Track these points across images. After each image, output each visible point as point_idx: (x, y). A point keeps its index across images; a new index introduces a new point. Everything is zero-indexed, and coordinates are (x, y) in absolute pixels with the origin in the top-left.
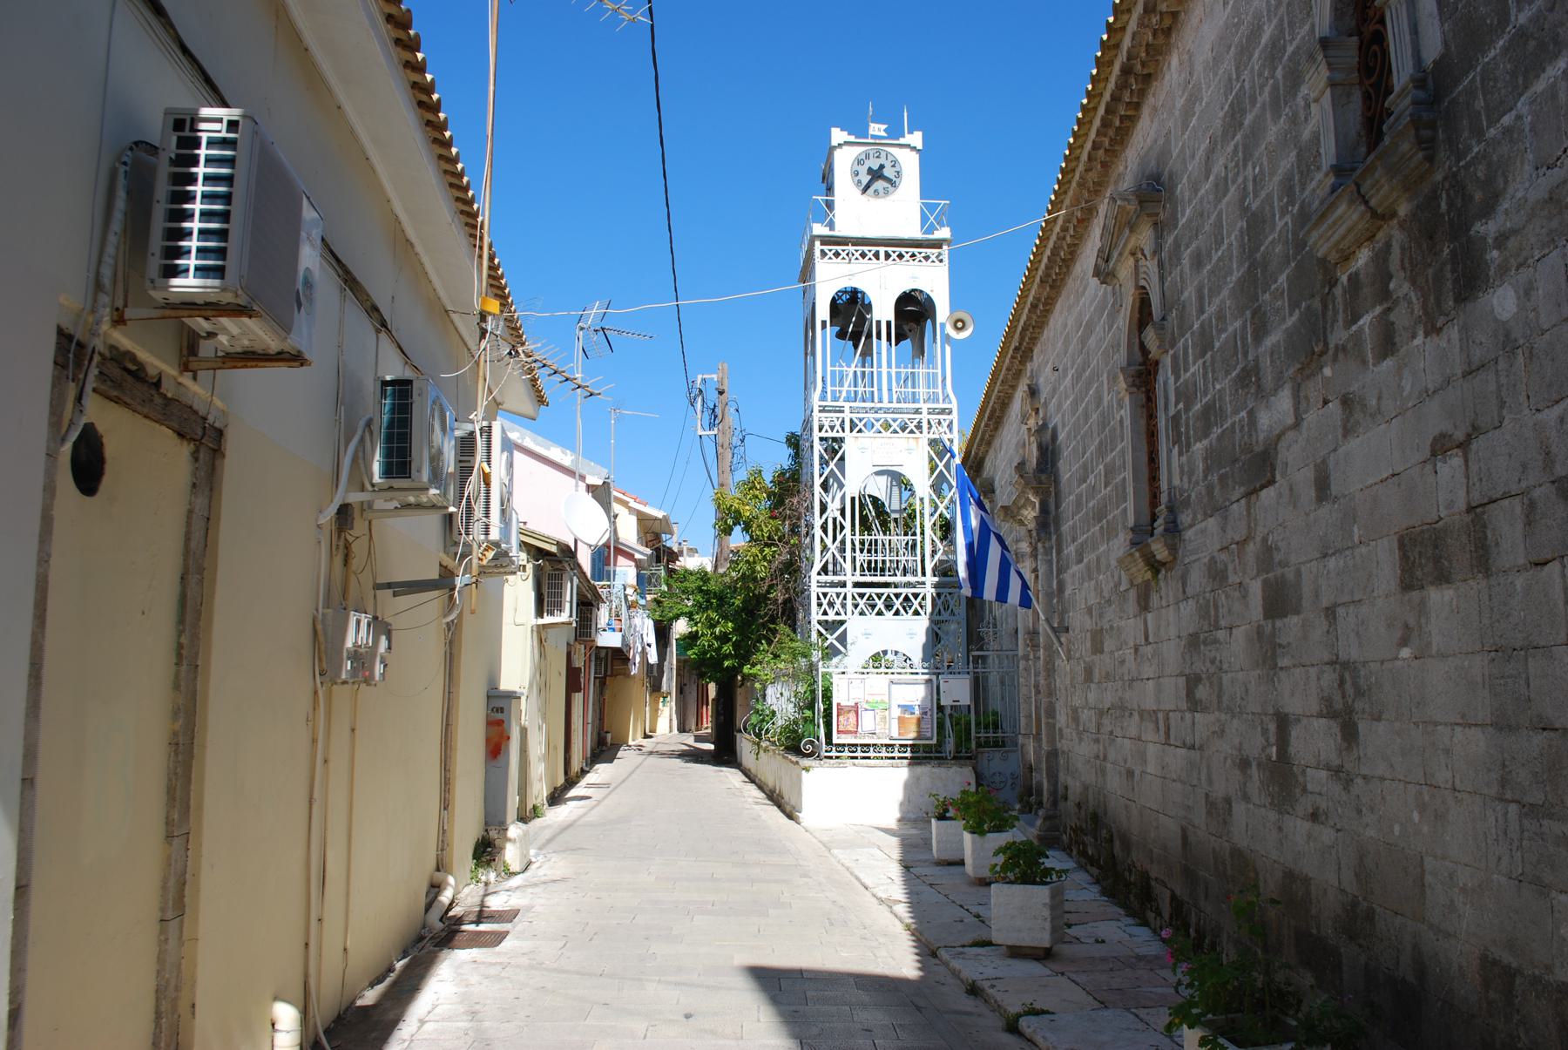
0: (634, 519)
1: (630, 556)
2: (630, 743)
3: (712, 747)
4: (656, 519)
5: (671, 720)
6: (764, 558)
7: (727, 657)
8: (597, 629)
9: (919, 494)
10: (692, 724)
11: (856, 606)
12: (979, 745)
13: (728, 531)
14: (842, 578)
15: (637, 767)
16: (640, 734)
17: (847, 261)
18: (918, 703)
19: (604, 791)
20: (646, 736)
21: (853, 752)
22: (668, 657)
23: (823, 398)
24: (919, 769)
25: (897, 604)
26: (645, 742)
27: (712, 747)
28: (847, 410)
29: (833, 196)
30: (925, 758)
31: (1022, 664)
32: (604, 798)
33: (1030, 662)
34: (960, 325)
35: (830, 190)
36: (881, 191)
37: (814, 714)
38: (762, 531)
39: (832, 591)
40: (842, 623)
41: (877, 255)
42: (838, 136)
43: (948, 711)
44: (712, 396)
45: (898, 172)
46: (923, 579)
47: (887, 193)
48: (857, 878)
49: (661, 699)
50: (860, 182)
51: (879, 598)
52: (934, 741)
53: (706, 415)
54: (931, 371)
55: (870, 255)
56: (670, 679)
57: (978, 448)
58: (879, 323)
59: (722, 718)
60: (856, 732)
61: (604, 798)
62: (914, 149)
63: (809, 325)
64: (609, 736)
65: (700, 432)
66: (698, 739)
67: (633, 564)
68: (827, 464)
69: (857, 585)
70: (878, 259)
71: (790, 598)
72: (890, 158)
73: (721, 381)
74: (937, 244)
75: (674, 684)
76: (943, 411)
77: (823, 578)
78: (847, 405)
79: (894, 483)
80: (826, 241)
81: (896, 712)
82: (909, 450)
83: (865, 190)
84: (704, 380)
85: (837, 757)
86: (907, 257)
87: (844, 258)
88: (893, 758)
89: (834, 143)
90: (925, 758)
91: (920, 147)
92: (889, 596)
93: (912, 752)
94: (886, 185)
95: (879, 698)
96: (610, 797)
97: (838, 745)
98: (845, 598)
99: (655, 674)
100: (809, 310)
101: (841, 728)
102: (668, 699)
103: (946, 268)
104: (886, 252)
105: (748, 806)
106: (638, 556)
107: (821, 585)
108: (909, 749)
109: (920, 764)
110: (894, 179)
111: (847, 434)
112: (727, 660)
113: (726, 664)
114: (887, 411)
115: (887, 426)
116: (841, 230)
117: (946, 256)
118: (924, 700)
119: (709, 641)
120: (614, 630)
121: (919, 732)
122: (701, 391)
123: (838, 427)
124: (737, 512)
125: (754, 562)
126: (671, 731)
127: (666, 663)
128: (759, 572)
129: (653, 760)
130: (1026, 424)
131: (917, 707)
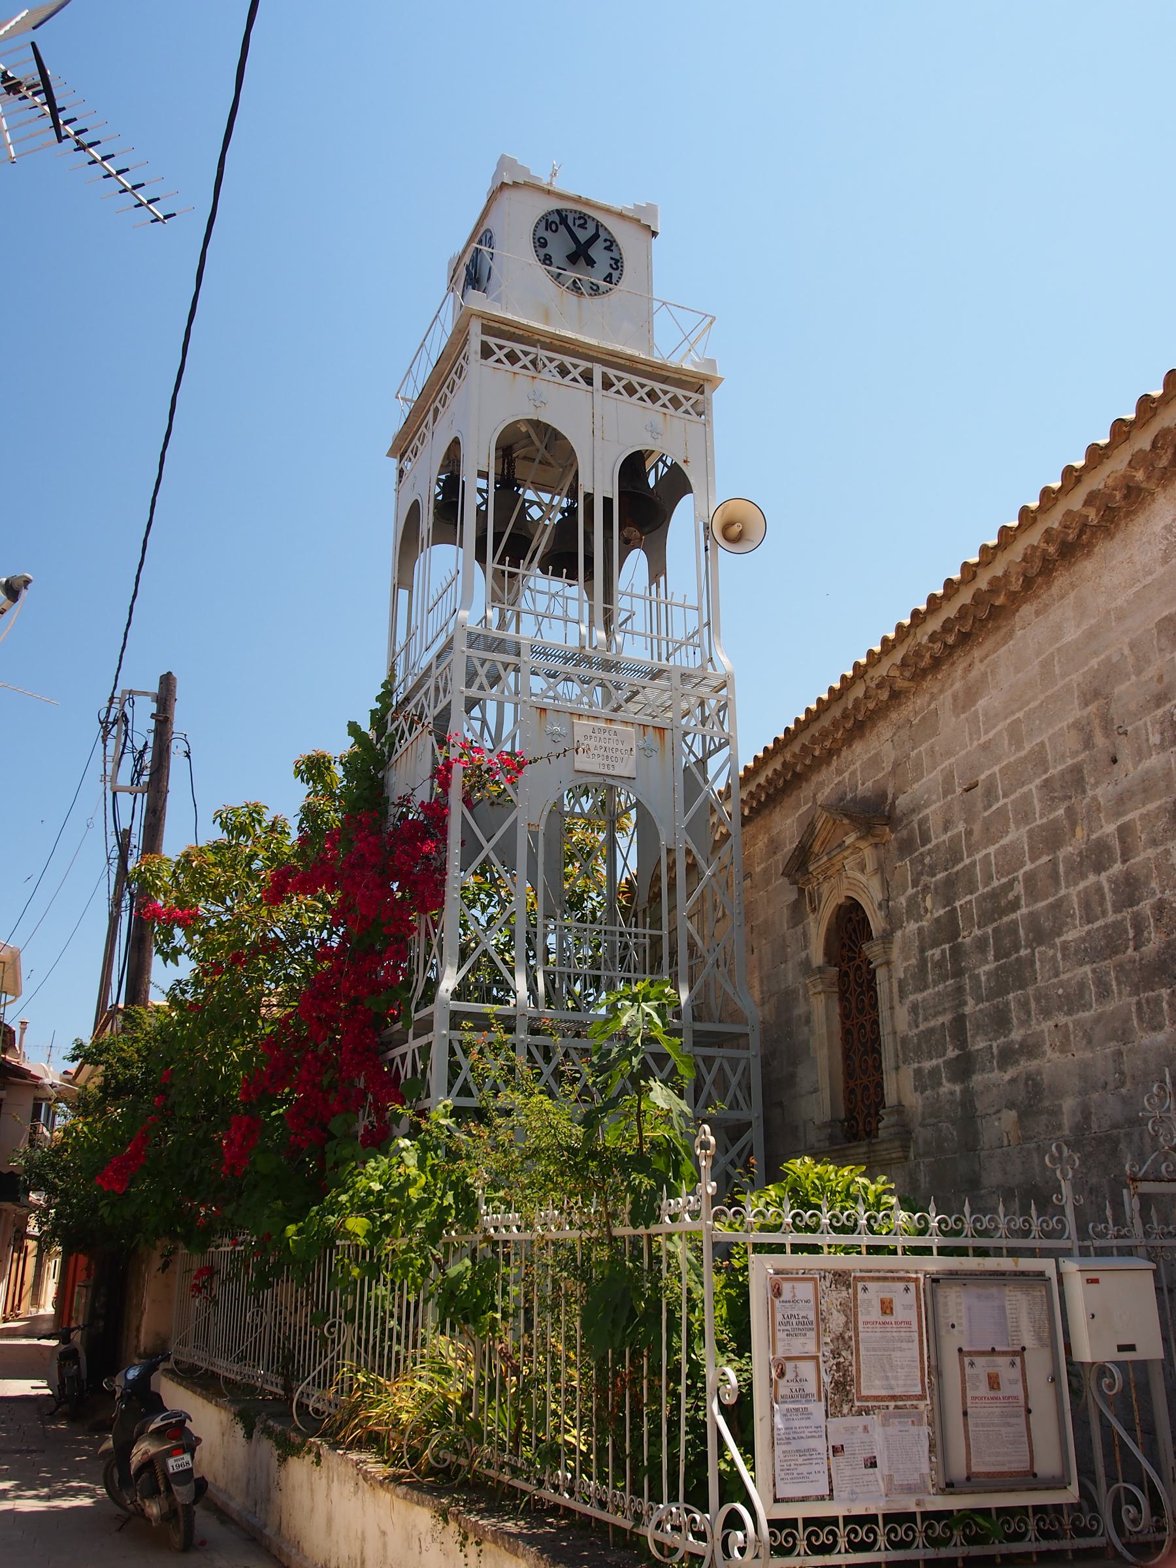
45: (617, 261)
52: (1071, 1494)
58: (589, 497)
59: (101, 1324)
92: (494, 666)
104: (604, 375)
126: (132, 784)
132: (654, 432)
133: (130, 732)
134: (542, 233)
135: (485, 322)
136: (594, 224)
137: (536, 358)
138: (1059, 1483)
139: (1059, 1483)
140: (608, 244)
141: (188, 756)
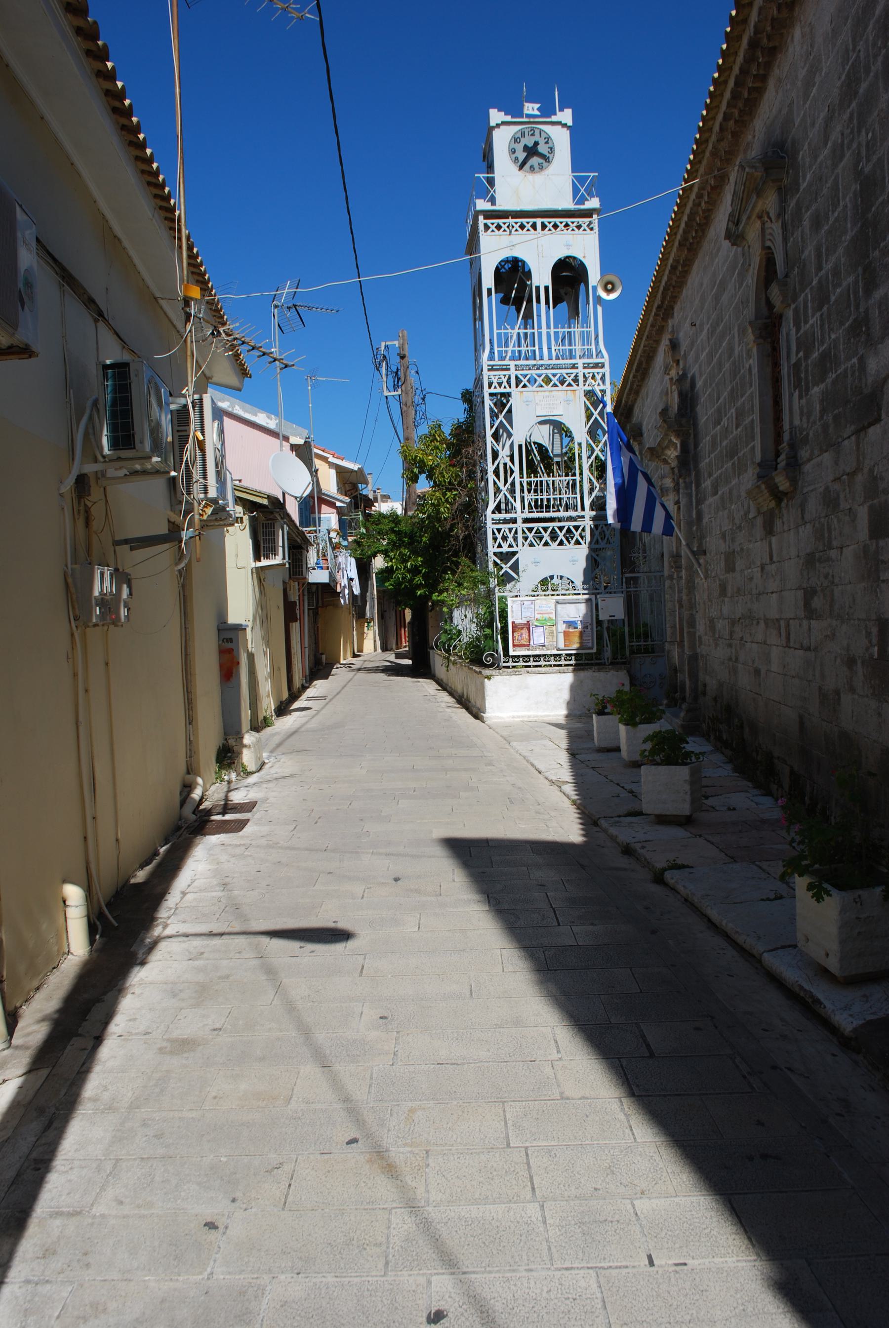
0: (333, 472)
1: (332, 505)
2: (342, 661)
3: (409, 662)
4: (352, 471)
5: (375, 641)
7: (419, 587)
8: (307, 568)
9: (577, 439)
11: (526, 539)
12: (632, 652)
13: (414, 479)
16: (349, 654)
17: (508, 233)
18: (580, 619)
21: (526, 662)
22: (369, 589)
23: (491, 358)
24: (582, 674)
26: (354, 660)
27: (409, 662)
28: (512, 368)
29: (494, 173)
30: (587, 664)
32: (322, 708)
33: (675, 581)
34: (609, 287)
35: (490, 168)
36: (536, 166)
37: (493, 631)
38: (444, 477)
40: (514, 554)
41: (534, 226)
43: (605, 625)
44: (395, 361)
45: (551, 148)
46: (583, 513)
47: (541, 168)
48: (532, 765)
49: (366, 625)
50: (517, 159)
52: (594, 650)
53: (390, 377)
55: (528, 226)
56: (372, 608)
57: (628, 398)
58: (538, 288)
60: (528, 645)
61: (322, 708)
62: (564, 125)
63: (477, 293)
64: (324, 657)
65: (386, 393)
67: (335, 511)
70: (535, 229)
71: (469, 534)
72: (544, 135)
73: (402, 347)
74: (588, 214)
75: (376, 611)
78: (512, 364)
79: (556, 431)
80: (489, 215)
81: (562, 627)
82: (568, 401)
83: (521, 167)
84: (387, 347)
85: (514, 667)
86: (561, 226)
87: (505, 231)
88: (561, 665)
90: (587, 664)
91: (570, 123)
93: (576, 660)
94: (540, 160)
95: (546, 616)
96: (327, 707)
98: (516, 532)
99: (359, 603)
100: (476, 280)
101: (516, 642)
102: (372, 624)
106: (338, 504)
107: (496, 522)
108: (573, 657)
109: (583, 670)
110: (548, 155)
111: (513, 390)
112: (420, 589)
114: (547, 367)
115: (547, 380)
117: (596, 224)
118: (585, 616)
119: (403, 574)
120: (322, 568)
121: (581, 643)
122: (384, 357)
124: (422, 461)
126: (375, 650)
127: (368, 594)
128: (443, 513)
129: (361, 675)
131: (579, 622)
132: (568, 246)
134: (513, 146)
138: (592, 648)
141: (417, 373)
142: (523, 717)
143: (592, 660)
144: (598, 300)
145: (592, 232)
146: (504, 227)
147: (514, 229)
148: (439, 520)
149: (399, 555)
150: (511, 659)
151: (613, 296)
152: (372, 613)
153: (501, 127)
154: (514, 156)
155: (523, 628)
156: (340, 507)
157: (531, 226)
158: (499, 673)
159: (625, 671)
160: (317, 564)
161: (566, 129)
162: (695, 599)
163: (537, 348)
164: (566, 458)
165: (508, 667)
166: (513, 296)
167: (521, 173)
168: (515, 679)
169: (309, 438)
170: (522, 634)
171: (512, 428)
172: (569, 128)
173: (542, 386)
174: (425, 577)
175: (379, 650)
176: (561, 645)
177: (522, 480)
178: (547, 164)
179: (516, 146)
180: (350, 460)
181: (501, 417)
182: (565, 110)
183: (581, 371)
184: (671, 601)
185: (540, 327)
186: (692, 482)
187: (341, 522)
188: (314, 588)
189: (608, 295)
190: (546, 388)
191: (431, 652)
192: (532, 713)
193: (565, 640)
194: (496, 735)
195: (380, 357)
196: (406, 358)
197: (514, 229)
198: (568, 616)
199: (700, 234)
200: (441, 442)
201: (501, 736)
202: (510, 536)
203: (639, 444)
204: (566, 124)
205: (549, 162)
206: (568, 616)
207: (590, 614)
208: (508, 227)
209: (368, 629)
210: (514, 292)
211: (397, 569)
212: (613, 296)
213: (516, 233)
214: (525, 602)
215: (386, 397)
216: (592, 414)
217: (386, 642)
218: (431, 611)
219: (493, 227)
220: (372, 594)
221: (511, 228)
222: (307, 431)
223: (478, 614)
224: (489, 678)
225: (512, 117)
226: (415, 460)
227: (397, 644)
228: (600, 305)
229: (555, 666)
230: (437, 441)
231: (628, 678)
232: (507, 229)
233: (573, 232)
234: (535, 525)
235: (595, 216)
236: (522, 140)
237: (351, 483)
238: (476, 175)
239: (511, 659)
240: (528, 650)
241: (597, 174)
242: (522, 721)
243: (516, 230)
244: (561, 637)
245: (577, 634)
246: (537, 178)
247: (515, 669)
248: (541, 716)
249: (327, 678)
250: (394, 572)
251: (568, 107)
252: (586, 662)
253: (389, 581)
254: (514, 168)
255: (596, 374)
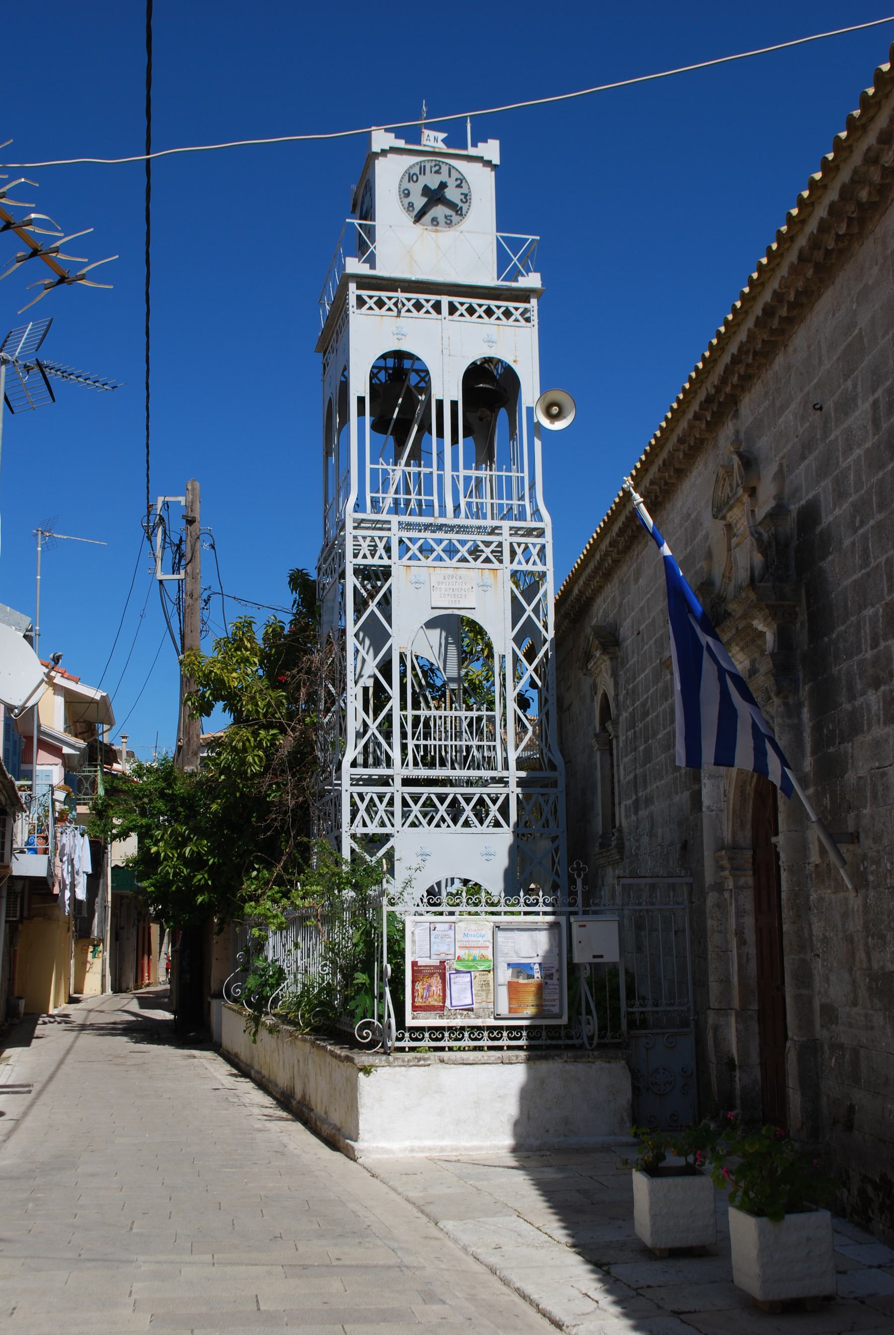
0: (60, 701)
1: (55, 751)
2: (52, 1011)
3: (168, 1016)
4: (91, 701)
5: (103, 976)
6: (259, 746)
7: (200, 889)
8: (12, 850)
9: (498, 650)
10: (130, 979)
11: (405, 815)
12: (631, 1025)
13: (205, 709)
14: (382, 771)
15: (68, 1052)
16: (62, 998)
17: (395, 313)
18: (538, 960)
19: (23, 1100)
20: (72, 1001)
21: (437, 1040)
22: (100, 892)
23: (359, 506)
24: (544, 1067)
25: (468, 811)
26: (71, 1009)
27: (168, 1016)
28: (394, 526)
29: (374, 221)
30: (548, 1047)
31: (711, 899)
32: (25, 1114)
33: (727, 895)
34: (555, 410)
35: (368, 213)
36: (442, 220)
37: (372, 978)
38: (257, 705)
39: (371, 791)
40: (387, 837)
41: (437, 307)
42: (381, 139)
43: (585, 974)
44: (177, 526)
45: (466, 195)
46: (505, 774)
47: (449, 223)
48: (525, 1297)
49: (91, 949)
50: (411, 205)
51: (442, 801)
52: (564, 1021)
53: (169, 552)
54: (504, 474)
55: (428, 306)
56: (102, 921)
57: (586, 584)
58: (440, 403)
59: (188, 976)
60: (442, 1008)
61: (25, 1114)
62: (488, 163)
63: (335, 408)
64: (22, 1003)
65: (160, 576)
66: (145, 1002)
67: (59, 761)
68: (365, 604)
69: (406, 782)
71: (305, 802)
72: (455, 175)
73: (190, 506)
74: (523, 295)
75: (109, 928)
76: (529, 532)
77: (360, 771)
78: (395, 519)
79: (450, 640)
80: (365, 282)
81: (505, 975)
82: (484, 586)
83: (418, 218)
84: (166, 505)
85: (412, 1049)
87: (390, 309)
88: (500, 1048)
89: (376, 148)
90: (548, 1047)
91: (496, 161)
93: (529, 1038)
94: (448, 212)
95: (476, 953)
96: (35, 1110)
97: (413, 1029)
98: (391, 803)
99: (85, 914)
100: (334, 391)
101: (419, 1002)
102: (101, 948)
103: (536, 330)
105: (258, 1125)
106: (66, 750)
107: (355, 782)
108: (524, 1033)
109: (545, 1058)
110: (460, 204)
111: (396, 563)
112: (202, 894)
113: (200, 899)
114: (451, 528)
115: (451, 551)
116: (383, 270)
117: (536, 313)
118: (548, 955)
119: (175, 867)
120: (35, 851)
121: (540, 1006)
122: (162, 519)
123: (381, 550)
124: (220, 681)
125: (245, 750)
126: (103, 990)
127: (98, 900)
128: (250, 765)
129: (88, 1039)
130: (724, 518)
131: (537, 967)
132: (490, 342)
133: (167, 532)
134: (406, 185)
135: (359, 280)
136: (447, 167)
137: (397, 301)
138: (559, 1016)
139: (559, 1016)
140: (459, 182)
141: (213, 547)
142: (430, 1149)
143: (559, 1038)
144: (536, 429)
145: (528, 324)
146: (390, 304)
147: (405, 308)
148: (242, 774)
149: (170, 836)
150: (407, 1035)
151: (559, 425)
152: (102, 930)
153: (389, 155)
154: (406, 201)
155: (432, 975)
156: (69, 755)
157: (432, 307)
158: (387, 1061)
159: (623, 1062)
160: (27, 843)
161: (489, 169)
162: (811, 930)
163: (435, 498)
164: (466, 685)
165: (401, 1050)
166: (395, 416)
167: (418, 227)
168: (416, 1073)
169: (31, 630)
170: (430, 986)
171: (391, 626)
172: (494, 167)
173: (441, 559)
174: (214, 871)
175: (109, 991)
176: (503, 1008)
177: (404, 713)
178: (459, 218)
179: (411, 186)
180: (89, 683)
181: (373, 606)
182: (489, 141)
183: (506, 538)
184: (720, 932)
185: (441, 466)
186: (800, 705)
187: (68, 779)
188: (19, 887)
189: (552, 423)
190: (448, 562)
191: (214, 1003)
192: (446, 1143)
193: (510, 999)
194: (393, 1195)
195: (155, 519)
196: (196, 524)
197: (405, 308)
198: (517, 953)
199: (856, 230)
200: (252, 650)
201: (408, 1200)
202: (381, 807)
203: (611, 659)
204: (490, 162)
205: (461, 215)
206: (517, 953)
207: (556, 951)
208: (396, 304)
209: (94, 957)
210: (397, 409)
211: (167, 857)
212: (559, 425)
213: (409, 314)
214: (437, 925)
215: (161, 582)
216: (524, 610)
217: (121, 976)
218: (218, 933)
219: (371, 303)
220: (105, 900)
221: (400, 306)
222: (29, 619)
223: (331, 947)
224: (367, 1071)
225: (406, 143)
226: (207, 676)
227: (136, 981)
228: (539, 439)
229: (491, 1048)
230: (247, 649)
231: (629, 1074)
232: (393, 308)
233: (498, 322)
234: (425, 790)
235: (534, 302)
236: (421, 177)
237: (85, 721)
238: (348, 220)
239: (407, 1035)
240: (441, 1017)
241: (538, 238)
242: (430, 1159)
243: (409, 311)
244: (503, 993)
245: (533, 989)
246: (446, 237)
247: (419, 1055)
248: (466, 1149)
249: (27, 1043)
250: (161, 863)
251: (494, 137)
252: (549, 1042)
253: (149, 878)
254: (407, 219)
255: (530, 546)
